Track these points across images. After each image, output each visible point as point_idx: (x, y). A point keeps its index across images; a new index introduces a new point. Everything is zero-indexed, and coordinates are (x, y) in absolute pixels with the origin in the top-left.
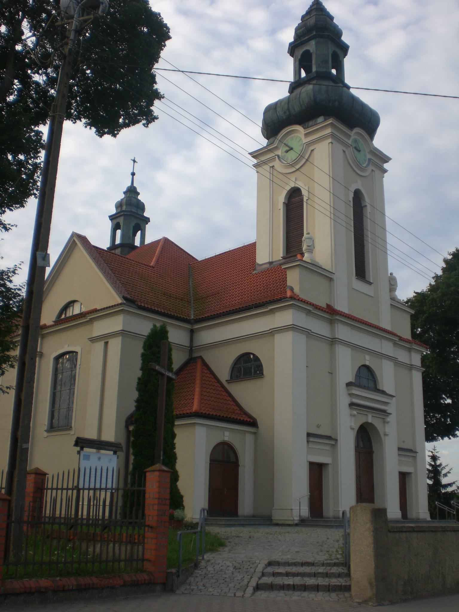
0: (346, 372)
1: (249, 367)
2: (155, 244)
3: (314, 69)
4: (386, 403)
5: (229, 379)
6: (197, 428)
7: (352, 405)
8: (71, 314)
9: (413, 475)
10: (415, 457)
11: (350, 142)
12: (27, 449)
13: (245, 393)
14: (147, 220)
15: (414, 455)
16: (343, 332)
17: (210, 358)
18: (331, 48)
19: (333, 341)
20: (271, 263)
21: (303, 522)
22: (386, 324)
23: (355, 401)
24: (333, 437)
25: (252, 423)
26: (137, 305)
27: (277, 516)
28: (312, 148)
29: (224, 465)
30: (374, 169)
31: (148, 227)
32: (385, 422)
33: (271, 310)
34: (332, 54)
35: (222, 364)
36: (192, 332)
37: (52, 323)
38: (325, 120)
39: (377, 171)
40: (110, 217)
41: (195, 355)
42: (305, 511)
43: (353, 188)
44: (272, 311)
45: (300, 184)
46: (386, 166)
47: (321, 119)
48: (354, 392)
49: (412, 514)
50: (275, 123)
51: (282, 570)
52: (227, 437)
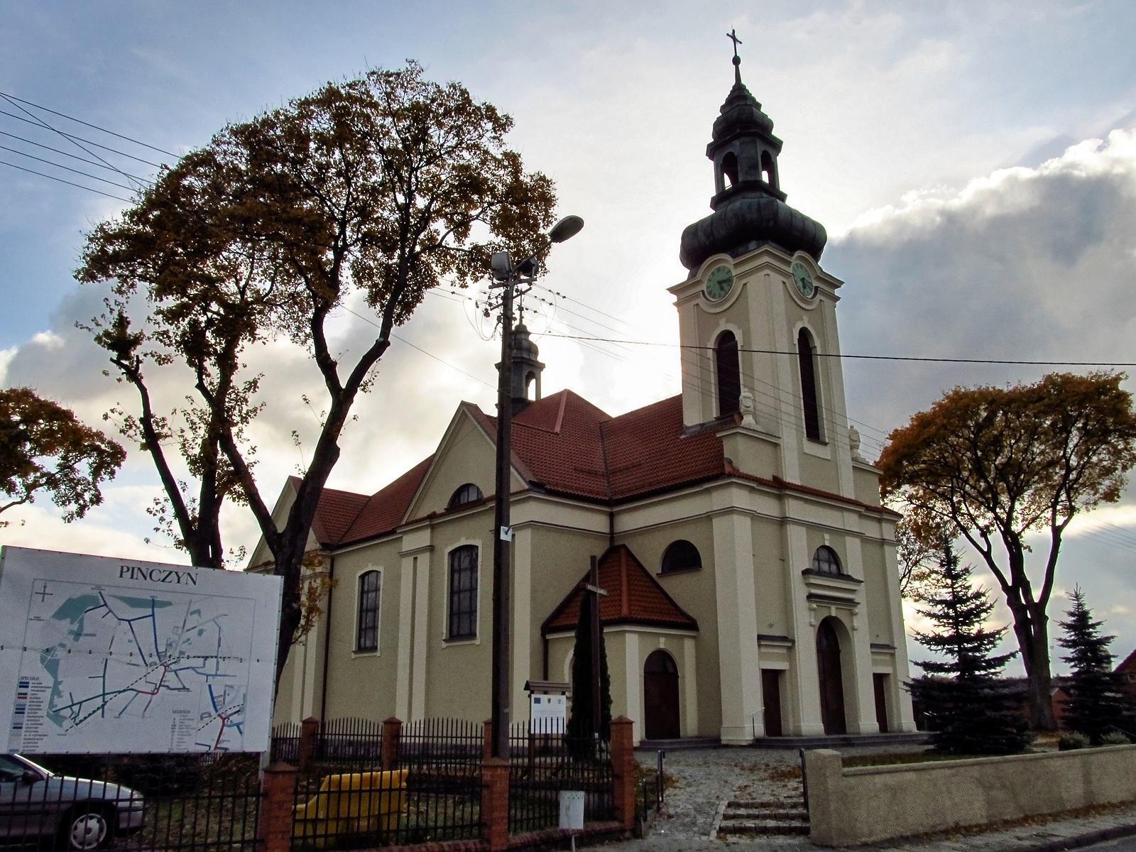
0: (801, 559)
1: (684, 557)
2: (555, 400)
3: (740, 179)
4: (853, 591)
5: (660, 572)
6: (627, 635)
7: (810, 597)
8: (466, 501)
9: (892, 677)
10: (893, 655)
11: (790, 270)
12: (508, 713)
13: (679, 588)
14: (542, 367)
15: (892, 651)
16: (795, 508)
17: (634, 547)
18: (761, 148)
19: (783, 521)
20: (702, 425)
21: (758, 744)
22: (848, 492)
23: (814, 591)
24: (789, 637)
25: (690, 625)
26: (546, 489)
27: (725, 739)
28: (744, 281)
29: (661, 674)
30: (822, 298)
31: (544, 375)
32: (852, 614)
33: (706, 489)
34: (762, 156)
35: (651, 556)
36: (612, 516)
37: (443, 511)
38: (758, 247)
39: (827, 302)
40: (496, 365)
41: (617, 543)
42: (760, 729)
43: (799, 325)
44: (708, 491)
45: (731, 327)
46: (837, 292)
47: (752, 245)
48: (813, 581)
49: (894, 724)
50: (700, 246)
51: (742, 811)
52: (662, 644)
